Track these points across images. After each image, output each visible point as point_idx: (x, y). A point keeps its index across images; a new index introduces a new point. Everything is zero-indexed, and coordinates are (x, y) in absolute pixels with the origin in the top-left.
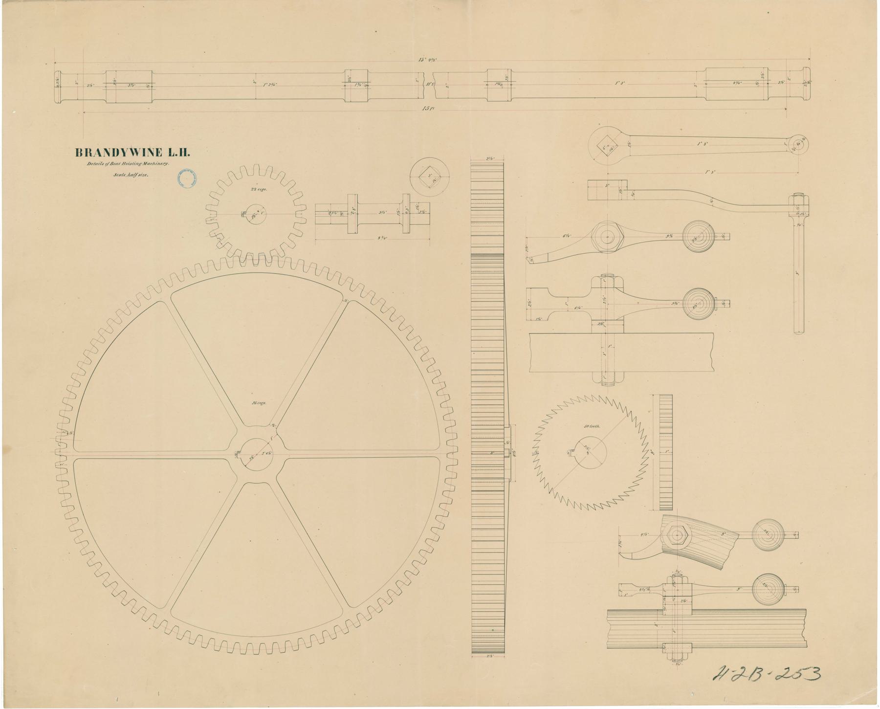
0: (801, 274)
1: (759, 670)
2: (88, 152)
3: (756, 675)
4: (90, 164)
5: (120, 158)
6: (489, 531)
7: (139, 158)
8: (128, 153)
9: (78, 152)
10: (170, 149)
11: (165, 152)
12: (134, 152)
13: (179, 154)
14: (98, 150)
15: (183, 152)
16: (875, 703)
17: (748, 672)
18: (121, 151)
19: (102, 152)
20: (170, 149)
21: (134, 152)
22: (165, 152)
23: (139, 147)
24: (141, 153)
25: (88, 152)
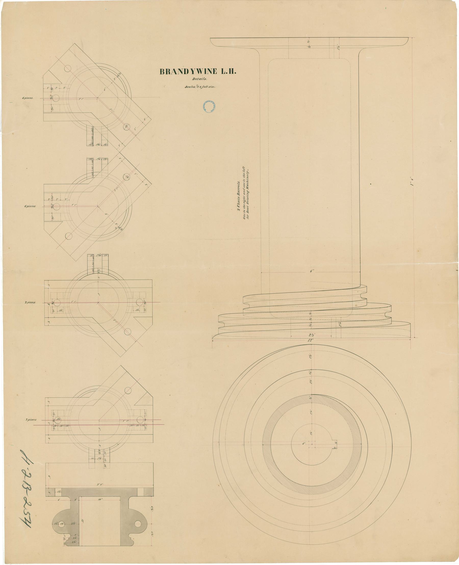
0: (310, 343)
1: (29, 489)
2: (168, 72)
3: (26, 486)
4: (194, 79)
6: (288, 313)
7: (202, 75)
8: (196, 71)
9: (161, 71)
10: (222, 69)
11: (219, 71)
12: (199, 71)
13: (228, 72)
14: (174, 69)
15: (231, 71)
17: (28, 480)
18: (190, 72)
19: (177, 71)
20: (222, 69)
21: (199, 71)
22: (219, 71)
23: (202, 68)
24: (203, 71)
25: (168, 72)
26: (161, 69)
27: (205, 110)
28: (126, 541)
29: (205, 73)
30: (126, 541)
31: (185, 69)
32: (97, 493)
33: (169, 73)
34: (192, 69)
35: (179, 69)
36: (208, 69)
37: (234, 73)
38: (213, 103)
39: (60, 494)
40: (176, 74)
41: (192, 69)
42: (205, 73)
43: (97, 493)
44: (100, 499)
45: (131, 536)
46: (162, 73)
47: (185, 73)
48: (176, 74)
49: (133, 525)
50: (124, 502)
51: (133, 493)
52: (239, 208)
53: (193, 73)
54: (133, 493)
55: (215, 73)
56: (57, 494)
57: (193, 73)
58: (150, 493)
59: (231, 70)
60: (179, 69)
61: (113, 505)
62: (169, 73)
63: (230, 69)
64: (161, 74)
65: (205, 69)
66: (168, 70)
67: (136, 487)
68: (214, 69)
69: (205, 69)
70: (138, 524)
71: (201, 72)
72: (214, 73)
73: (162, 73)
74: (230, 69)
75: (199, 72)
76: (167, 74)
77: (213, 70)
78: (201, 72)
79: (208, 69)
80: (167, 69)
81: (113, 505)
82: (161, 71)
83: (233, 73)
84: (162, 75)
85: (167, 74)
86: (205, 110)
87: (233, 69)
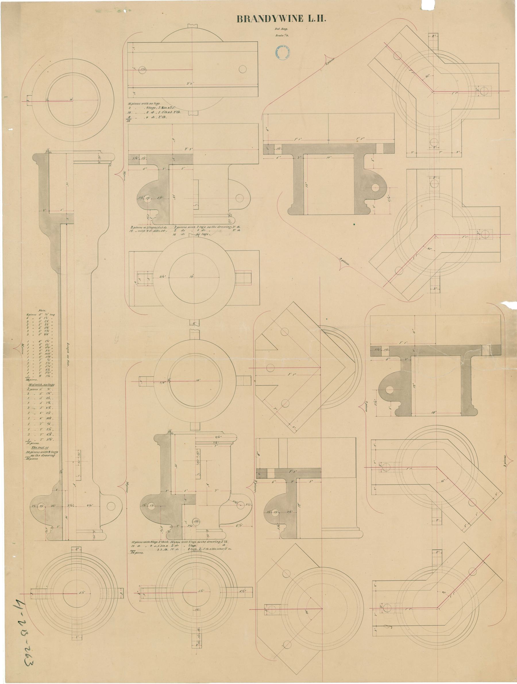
2: (246, 19)
8: (278, 19)
10: (310, 16)
11: (305, 18)
12: (282, 18)
13: (317, 20)
14: (254, 16)
15: (320, 18)
20: (310, 16)
21: (282, 18)
22: (305, 18)
24: (287, 19)
25: (246, 19)
26: (238, 16)
28: (362, 209)
29: (290, 21)
30: (362, 209)
31: (266, 16)
32: (328, 150)
33: (249, 21)
35: (260, 16)
36: (294, 16)
37: (324, 20)
39: (280, 151)
40: (256, 21)
42: (290, 21)
43: (328, 150)
44: (329, 158)
45: (366, 202)
46: (240, 20)
47: (266, 21)
48: (256, 21)
49: (369, 189)
50: (359, 165)
51: (371, 149)
53: (275, 21)
54: (371, 149)
55: (301, 20)
56: (276, 152)
57: (275, 21)
58: (390, 149)
59: (320, 17)
60: (260, 16)
61: (345, 164)
62: (249, 21)
63: (318, 16)
64: (238, 21)
67: (374, 142)
68: (300, 16)
69: (289, 16)
70: (375, 188)
71: (284, 20)
72: (300, 21)
73: (240, 20)
74: (318, 16)
75: (282, 20)
76: (245, 21)
77: (298, 16)
78: (284, 20)
79: (294, 16)
80: (245, 16)
81: (345, 164)
82: (239, 19)
83: (322, 21)
84: (240, 23)
85: (245, 21)
87: (322, 16)
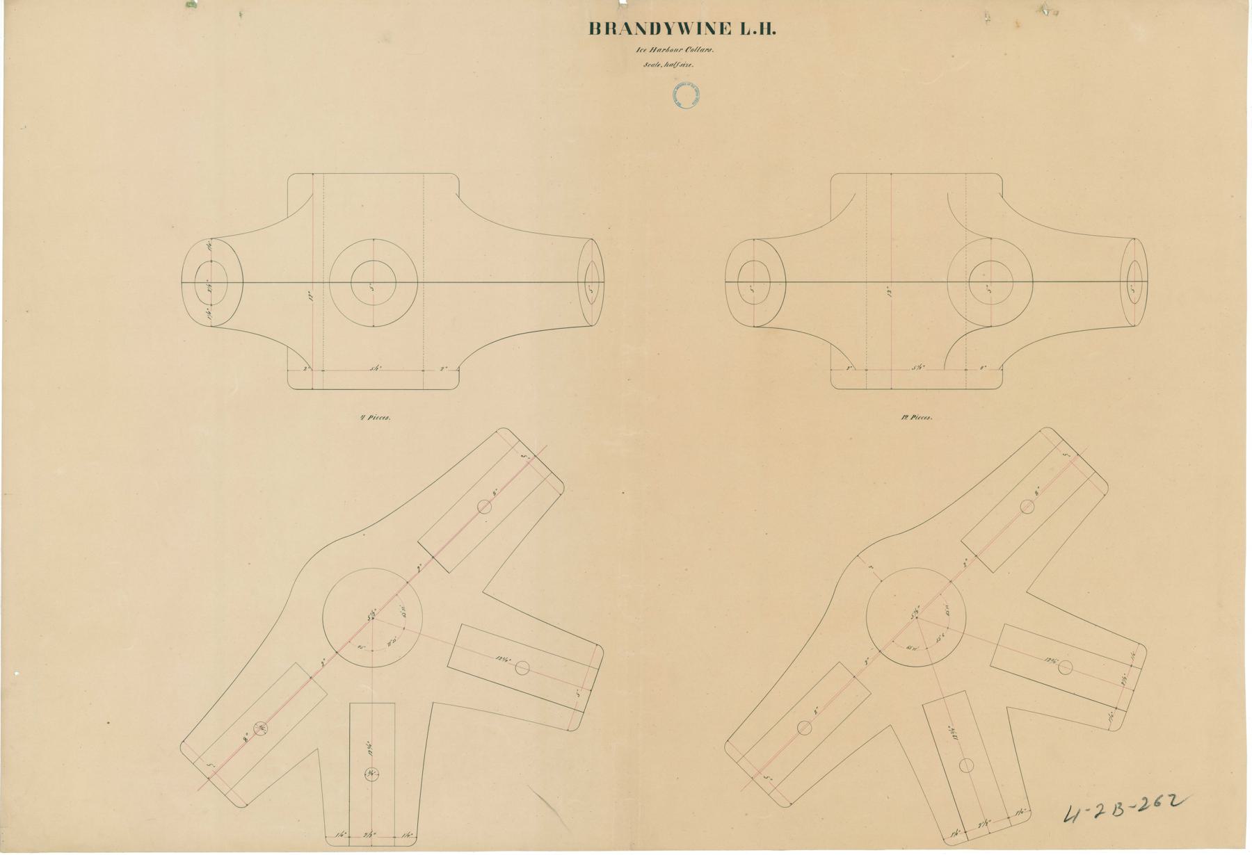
2: (611, 28)
3: (1118, 812)
5: (662, 39)
7: (692, 39)
12: (684, 28)
13: (759, 32)
16: (1240, 844)
19: (633, 28)
21: (684, 28)
24: (694, 29)
25: (611, 28)
27: (679, 105)
34: (667, 24)
38: (697, 91)
41: (667, 24)
52: (1109, 809)
53: (670, 33)
57: (670, 33)
65: (699, 24)
66: (611, 26)
69: (699, 24)
74: (592, 24)
82: (594, 28)
84: (595, 35)
86: (679, 105)
